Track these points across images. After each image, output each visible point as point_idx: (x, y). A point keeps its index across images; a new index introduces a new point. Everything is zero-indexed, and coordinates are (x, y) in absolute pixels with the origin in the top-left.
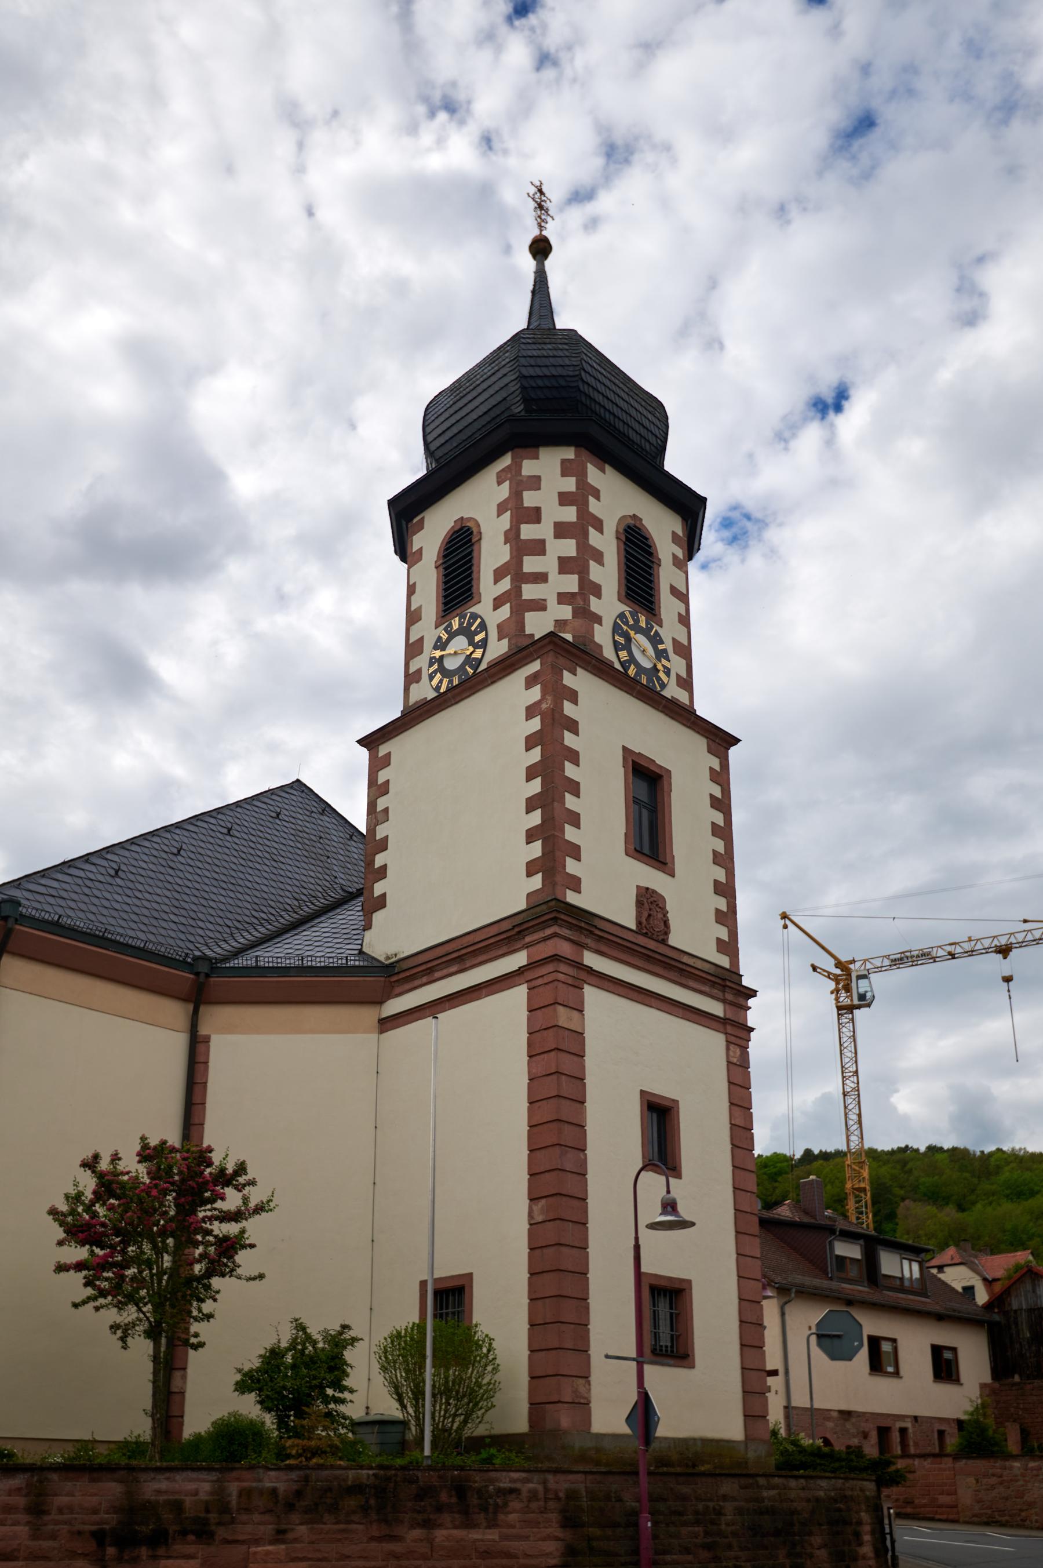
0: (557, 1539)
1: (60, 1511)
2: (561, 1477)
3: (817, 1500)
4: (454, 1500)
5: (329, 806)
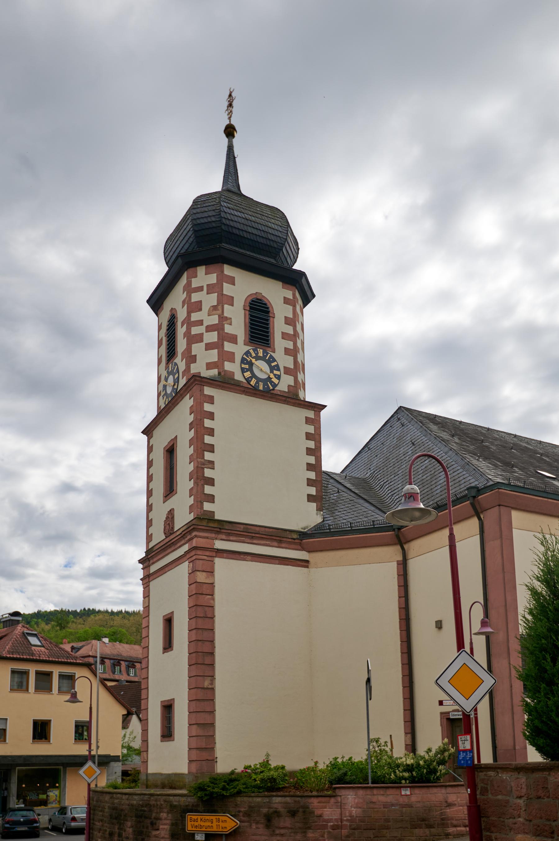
3: (132, 805)
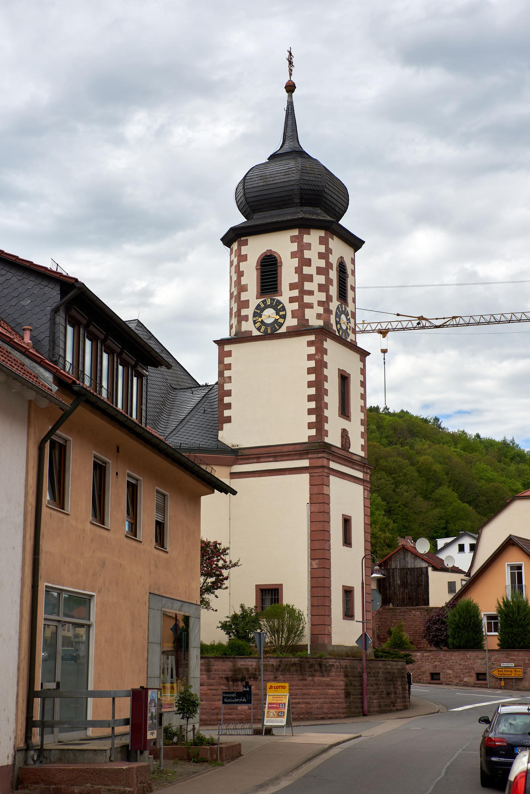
0: (343, 681)
1: (215, 671)
2: (344, 661)
4: (319, 668)
5: (143, 325)
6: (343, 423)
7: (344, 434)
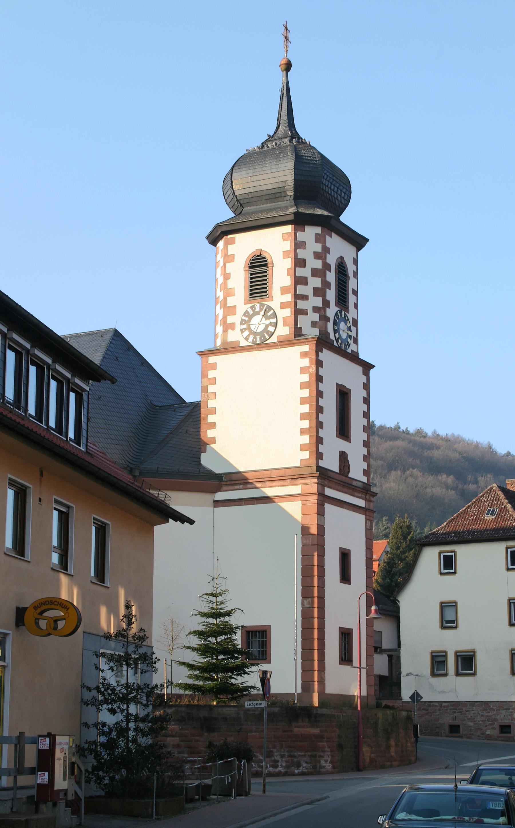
6: (342, 445)
7: (343, 457)
